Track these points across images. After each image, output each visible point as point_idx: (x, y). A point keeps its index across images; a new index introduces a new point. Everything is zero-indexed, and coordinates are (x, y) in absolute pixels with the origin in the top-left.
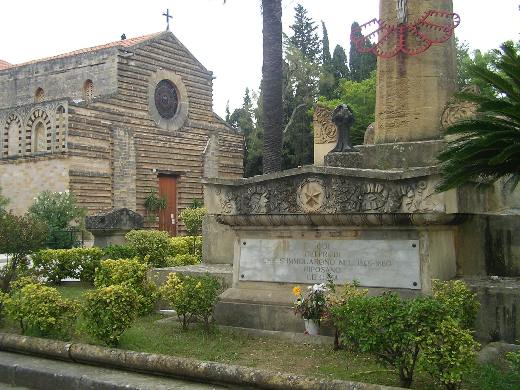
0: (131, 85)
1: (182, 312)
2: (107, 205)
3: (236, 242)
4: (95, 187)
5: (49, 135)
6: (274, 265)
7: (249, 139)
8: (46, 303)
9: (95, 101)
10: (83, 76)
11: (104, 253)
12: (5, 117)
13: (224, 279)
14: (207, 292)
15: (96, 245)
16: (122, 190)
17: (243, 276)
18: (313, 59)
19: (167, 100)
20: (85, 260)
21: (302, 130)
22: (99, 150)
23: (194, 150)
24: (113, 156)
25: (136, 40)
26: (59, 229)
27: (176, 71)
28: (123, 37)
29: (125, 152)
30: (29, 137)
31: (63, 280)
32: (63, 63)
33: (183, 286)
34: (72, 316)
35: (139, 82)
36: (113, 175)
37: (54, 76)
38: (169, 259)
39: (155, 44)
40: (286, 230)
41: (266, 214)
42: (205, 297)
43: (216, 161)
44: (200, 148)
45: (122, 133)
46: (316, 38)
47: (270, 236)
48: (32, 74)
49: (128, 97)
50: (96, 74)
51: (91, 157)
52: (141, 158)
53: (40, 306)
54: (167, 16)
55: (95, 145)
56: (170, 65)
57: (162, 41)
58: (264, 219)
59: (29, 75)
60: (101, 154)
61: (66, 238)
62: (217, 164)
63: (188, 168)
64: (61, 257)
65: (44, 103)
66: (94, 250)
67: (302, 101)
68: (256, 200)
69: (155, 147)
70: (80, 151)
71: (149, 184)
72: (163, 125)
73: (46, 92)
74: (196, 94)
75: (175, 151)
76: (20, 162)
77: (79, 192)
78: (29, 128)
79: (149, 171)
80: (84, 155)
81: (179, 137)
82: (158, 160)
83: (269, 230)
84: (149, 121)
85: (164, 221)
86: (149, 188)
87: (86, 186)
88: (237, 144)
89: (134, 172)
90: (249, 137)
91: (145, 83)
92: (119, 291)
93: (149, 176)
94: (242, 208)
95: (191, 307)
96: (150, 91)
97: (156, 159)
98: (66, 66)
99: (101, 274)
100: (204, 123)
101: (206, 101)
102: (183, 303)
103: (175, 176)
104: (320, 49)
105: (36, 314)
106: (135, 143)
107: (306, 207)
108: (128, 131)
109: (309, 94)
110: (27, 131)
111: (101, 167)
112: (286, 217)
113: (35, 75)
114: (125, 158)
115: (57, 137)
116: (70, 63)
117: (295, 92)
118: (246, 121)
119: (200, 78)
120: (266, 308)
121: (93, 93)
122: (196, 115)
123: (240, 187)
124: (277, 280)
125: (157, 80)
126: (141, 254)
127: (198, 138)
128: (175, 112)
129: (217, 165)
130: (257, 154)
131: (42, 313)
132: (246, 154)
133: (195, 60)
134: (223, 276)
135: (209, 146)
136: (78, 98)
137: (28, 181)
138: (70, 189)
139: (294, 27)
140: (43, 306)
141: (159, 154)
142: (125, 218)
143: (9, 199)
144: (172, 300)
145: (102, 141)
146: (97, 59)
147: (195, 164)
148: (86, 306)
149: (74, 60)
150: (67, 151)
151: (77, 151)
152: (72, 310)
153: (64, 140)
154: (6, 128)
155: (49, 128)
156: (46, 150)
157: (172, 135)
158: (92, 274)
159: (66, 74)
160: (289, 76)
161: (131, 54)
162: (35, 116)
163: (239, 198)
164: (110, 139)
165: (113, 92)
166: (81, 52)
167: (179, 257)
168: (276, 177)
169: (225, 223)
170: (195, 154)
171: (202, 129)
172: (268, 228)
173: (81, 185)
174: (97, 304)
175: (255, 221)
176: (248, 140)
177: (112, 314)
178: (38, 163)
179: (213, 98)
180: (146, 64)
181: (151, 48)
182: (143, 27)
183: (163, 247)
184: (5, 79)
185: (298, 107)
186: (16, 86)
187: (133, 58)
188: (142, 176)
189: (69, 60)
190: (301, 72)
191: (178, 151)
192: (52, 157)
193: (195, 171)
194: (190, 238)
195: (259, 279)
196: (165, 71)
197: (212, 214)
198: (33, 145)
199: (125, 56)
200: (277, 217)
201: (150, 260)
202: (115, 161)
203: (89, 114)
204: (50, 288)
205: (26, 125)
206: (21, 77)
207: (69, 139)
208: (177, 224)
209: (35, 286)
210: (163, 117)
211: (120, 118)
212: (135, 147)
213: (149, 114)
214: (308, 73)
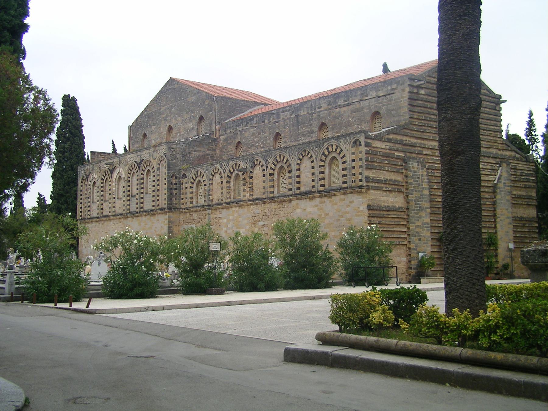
0: (422, 115)
4: (392, 221)
5: (344, 169)
9: (389, 132)
10: (370, 108)
12: (296, 153)
16: (418, 224)
22: (394, 183)
24: (407, 189)
28: (385, 68)
29: (419, 184)
30: (323, 172)
32: (348, 98)
36: (408, 209)
37: (338, 110)
43: (508, 192)
44: (491, 178)
45: (415, 165)
48: (315, 109)
49: (419, 127)
50: (383, 106)
52: (433, 190)
59: (311, 110)
60: (396, 187)
62: (509, 195)
70: (377, 185)
73: (330, 126)
74: (485, 121)
76: (314, 197)
78: (322, 164)
87: (383, 221)
88: (529, 172)
89: (427, 205)
100: (494, 151)
101: (495, 128)
106: (428, 175)
110: (321, 166)
111: (395, 200)
113: (318, 110)
114: (419, 191)
115: (353, 171)
116: (356, 96)
119: (488, 103)
127: (489, 167)
129: (509, 196)
135: (500, 176)
137: (323, 216)
146: (385, 89)
149: (359, 93)
151: (373, 185)
153: (361, 174)
155: (343, 163)
156: (341, 184)
159: (351, 107)
161: (423, 82)
162: (328, 151)
164: (404, 171)
165: (404, 122)
170: (486, 185)
171: (492, 157)
173: (379, 219)
178: (333, 198)
184: (287, 116)
186: (298, 122)
188: (435, 209)
189: (354, 93)
192: (348, 191)
193: (487, 203)
198: (327, 180)
199: (415, 84)
202: (410, 194)
203: (384, 147)
206: (302, 113)
207: (366, 173)
212: (428, 179)
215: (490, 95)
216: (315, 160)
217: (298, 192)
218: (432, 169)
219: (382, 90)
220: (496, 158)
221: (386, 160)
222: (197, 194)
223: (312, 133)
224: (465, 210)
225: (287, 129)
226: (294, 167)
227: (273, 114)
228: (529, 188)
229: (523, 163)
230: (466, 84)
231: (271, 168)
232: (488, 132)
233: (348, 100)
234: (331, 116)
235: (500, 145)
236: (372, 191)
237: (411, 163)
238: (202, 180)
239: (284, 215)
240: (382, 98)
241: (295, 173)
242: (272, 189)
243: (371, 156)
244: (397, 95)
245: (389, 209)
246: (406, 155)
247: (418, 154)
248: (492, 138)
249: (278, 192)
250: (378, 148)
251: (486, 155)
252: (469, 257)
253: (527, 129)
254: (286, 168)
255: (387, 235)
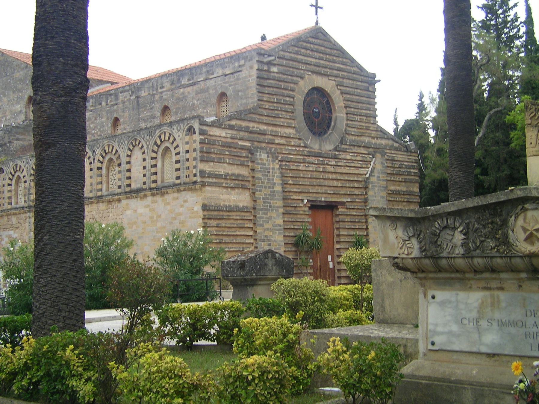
0: (274, 97)
1: (350, 393)
2: (248, 246)
3: (421, 296)
4: (234, 224)
5: (177, 162)
6: (478, 329)
7: (426, 158)
8: (170, 378)
9: (230, 118)
10: (216, 89)
11: (245, 309)
12: (126, 142)
13: (405, 346)
14: (383, 366)
15: (235, 297)
16: (267, 226)
17: (433, 344)
18: (513, 47)
19: (319, 112)
20: (222, 317)
21: (498, 143)
22: (237, 178)
23: (354, 174)
24: (254, 185)
25: (279, 41)
26: (191, 276)
27: (328, 76)
28: (263, 38)
29: (269, 179)
30: (155, 166)
31: (195, 343)
33: (351, 355)
34: (205, 397)
35: (284, 91)
36: (254, 208)
37: (182, 90)
38: (329, 316)
39: (301, 43)
40: (495, 279)
41: (464, 256)
42: (382, 373)
43: (383, 187)
44: (362, 171)
45: (264, 156)
46: (516, 19)
47: (470, 288)
48: (157, 90)
50: (230, 86)
51: (227, 187)
52: (288, 186)
53: (163, 382)
54: (317, 7)
55: (232, 172)
56: (321, 69)
57: (310, 39)
58: (460, 263)
60: (240, 182)
61: (200, 287)
63: (347, 196)
64: (193, 313)
65: (171, 124)
66: (233, 305)
67: (497, 105)
68: (447, 237)
69: (305, 172)
70: (214, 180)
71: (300, 218)
72: (315, 145)
74: (354, 104)
75: (330, 176)
76: (145, 196)
77: (214, 230)
78: (154, 155)
79: (298, 201)
80: (219, 185)
81: (335, 157)
82: (310, 188)
83: (469, 279)
84: (297, 140)
85: (319, 264)
86: (299, 224)
87: (223, 223)
88: (410, 164)
89: (280, 203)
90: (426, 154)
91: (291, 93)
92: (265, 364)
93: (298, 209)
94: (428, 248)
95: (362, 387)
96: (296, 103)
97: (307, 187)
98: (195, 77)
99: (242, 337)
100: (367, 139)
101: (368, 112)
102: (352, 381)
103: (331, 207)
104: (521, 33)
105: (158, 393)
106: (281, 168)
107: (523, 245)
108: (271, 153)
109: (507, 94)
110: (153, 158)
111: (240, 198)
112: (494, 260)
113: (160, 90)
114: (269, 187)
115: (187, 164)
116: (201, 74)
117: (487, 92)
118: (421, 134)
119: (358, 83)
120: (470, 392)
121: (227, 109)
122: (355, 130)
123: (424, 219)
124: (484, 349)
125: (305, 88)
126: (293, 310)
127: (359, 158)
128: (329, 127)
129: (384, 193)
130: (437, 175)
131: (166, 393)
132: (422, 176)
133: (353, 61)
134: (404, 342)
135: (373, 168)
136: (211, 116)
137: (155, 218)
138: (203, 227)
139: (484, 7)
140: (167, 383)
141: (310, 180)
142: (270, 263)
143: (132, 241)
144: (336, 376)
145: (240, 167)
146: (232, 66)
147: (357, 192)
148: (221, 383)
149: (204, 70)
150: (199, 180)
151: (210, 180)
152: (205, 388)
153: (195, 167)
154: (128, 156)
155: (177, 154)
157: (326, 155)
158: (231, 336)
159: (195, 87)
160: (478, 72)
161: (273, 58)
162: (161, 140)
163: (422, 234)
164: (250, 164)
165: (252, 106)
166: (213, 59)
167: (341, 314)
168: (476, 205)
169: (405, 269)
170: (356, 179)
171: (364, 147)
172: (467, 275)
174: (236, 381)
175: (447, 267)
176: (424, 159)
177: (255, 396)
178: (166, 197)
179: (376, 106)
180: (291, 69)
181: (296, 49)
182: (286, 22)
183: (320, 300)
185: (491, 112)
186: (138, 105)
187: (275, 62)
188: (290, 209)
190: (494, 65)
191: (334, 176)
192: (182, 188)
193: (357, 200)
194: (354, 287)
195: (456, 348)
196: (314, 77)
197: (385, 257)
198: (159, 175)
200: (480, 260)
201: (305, 318)
202: (257, 190)
203: (224, 135)
204: (176, 358)
205: (151, 150)
206: (143, 94)
207: (202, 166)
208: (336, 269)
209: (156, 356)
210: (314, 134)
211: (262, 137)
212: (281, 173)
213: (297, 131)
214: (504, 67)
215: (362, 74)
216: (146, 152)
217: (128, 189)
218: (287, 161)
219: (229, 67)
220: (369, 148)
221: (228, 151)
222: (16, 193)
223: (154, 118)
224: (54, 216)
225: (126, 114)
226: (124, 159)
227: (111, 95)
228: (409, 182)
229: (402, 153)
230: (59, 58)
231: (99, 160)
232: (359, 117)
233: (193, 78)
234: (175, 98)
235: (374, 132)
236: (208, 188)
237: (258, 154)
238: (22, 176)
239: (113, 217)
240: (229, 76)
241: (125, 166)
242: (99, 187)
243: (208, 146)
244: (245, 73)
245: (230, 210)
246: (253, 144)
247: (268, 143)
248: (363, 124)
249: (107, 190)
250: (216, 136)
251: (355, 144)
252: (55, 276)
253: (417, 113)
254: (115, 160)
255: (227, 239)
